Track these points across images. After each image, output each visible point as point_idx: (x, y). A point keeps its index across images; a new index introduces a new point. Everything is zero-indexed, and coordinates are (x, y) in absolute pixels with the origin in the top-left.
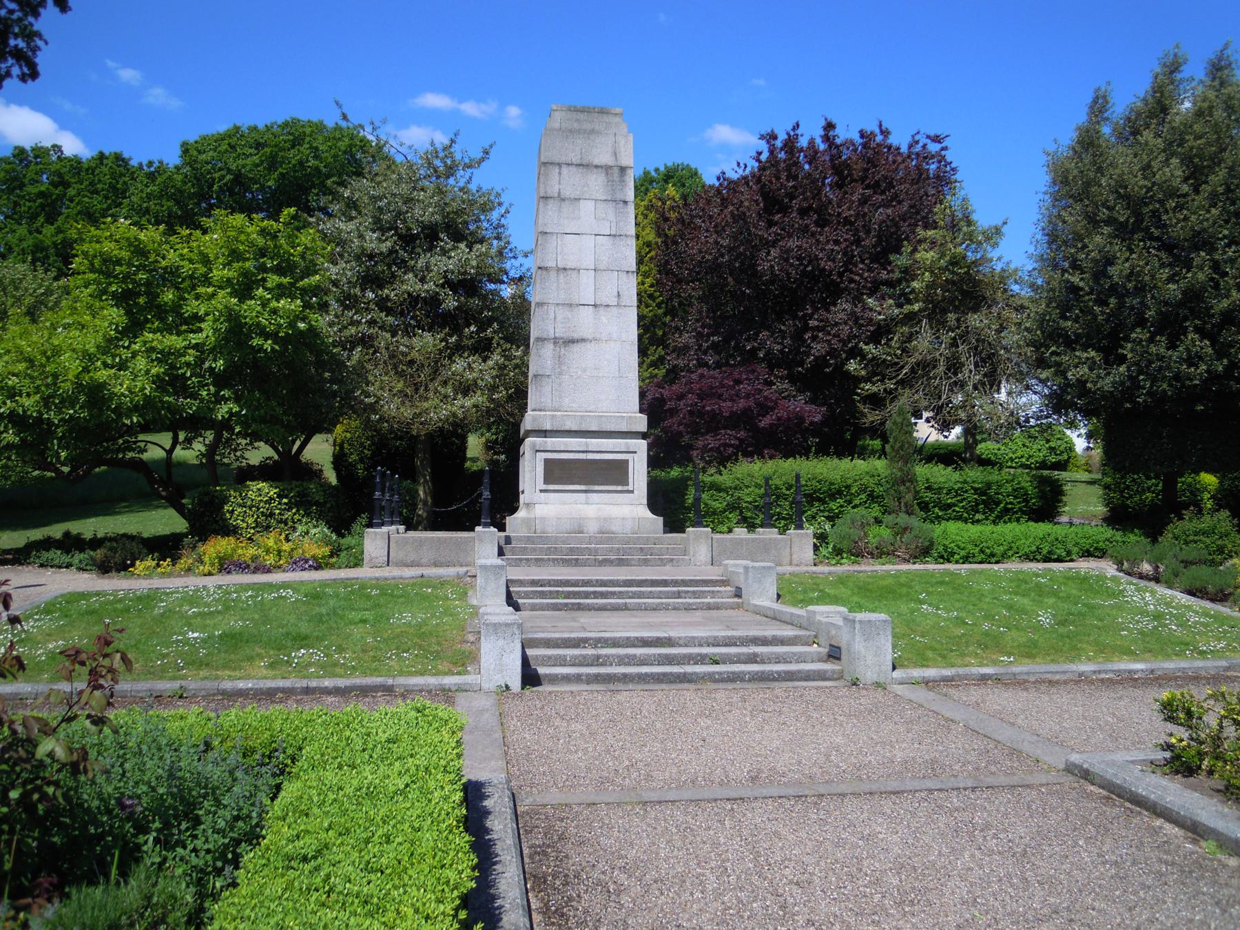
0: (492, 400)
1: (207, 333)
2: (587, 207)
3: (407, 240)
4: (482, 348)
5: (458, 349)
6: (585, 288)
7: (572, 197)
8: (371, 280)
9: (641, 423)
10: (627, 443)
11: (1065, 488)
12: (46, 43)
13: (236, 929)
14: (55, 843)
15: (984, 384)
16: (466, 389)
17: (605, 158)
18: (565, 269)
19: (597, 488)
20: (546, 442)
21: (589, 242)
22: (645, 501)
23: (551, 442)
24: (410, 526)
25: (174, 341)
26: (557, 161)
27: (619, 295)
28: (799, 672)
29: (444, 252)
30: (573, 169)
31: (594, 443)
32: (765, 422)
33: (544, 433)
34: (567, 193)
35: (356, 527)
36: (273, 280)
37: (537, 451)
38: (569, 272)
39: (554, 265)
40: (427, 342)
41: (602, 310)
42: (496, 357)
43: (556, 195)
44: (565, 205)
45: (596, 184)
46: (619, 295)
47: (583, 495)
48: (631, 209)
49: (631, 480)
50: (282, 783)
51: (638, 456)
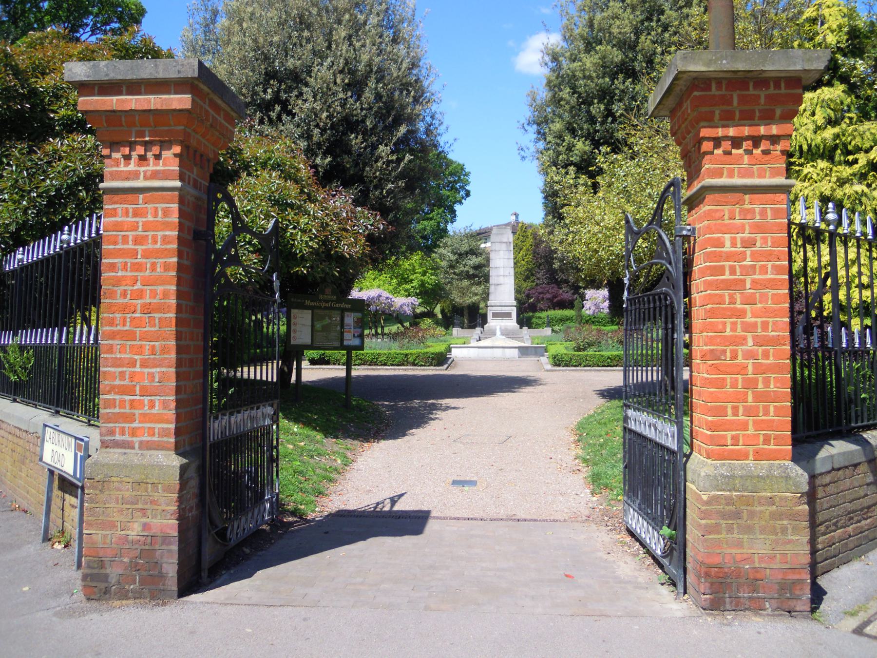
0: (396, 402)
1: (415, 283)
2: (501, 253)
3: (460, 255)
4: (479, 284)
5: (472, 284)
6: (501, 272)
8: (452, 267)
9: (515, 303)
14: (265, 530)
15: (112, 432)
16: (476, 294)
17: (505, 240)
21: (502, 260)
23: (493, 308)
24: (462, 328)
25: (408, 286)
29: (470, 259)
31: (503, 308)
32: (556, 300)
33: (492, 306)
35: (450, 328)
36: (430, 271)
40: (466, 283)
42: (483, 286)
45: (504, 246)
48: (512, 252)
50: (449, 350)
51: (514, 312)
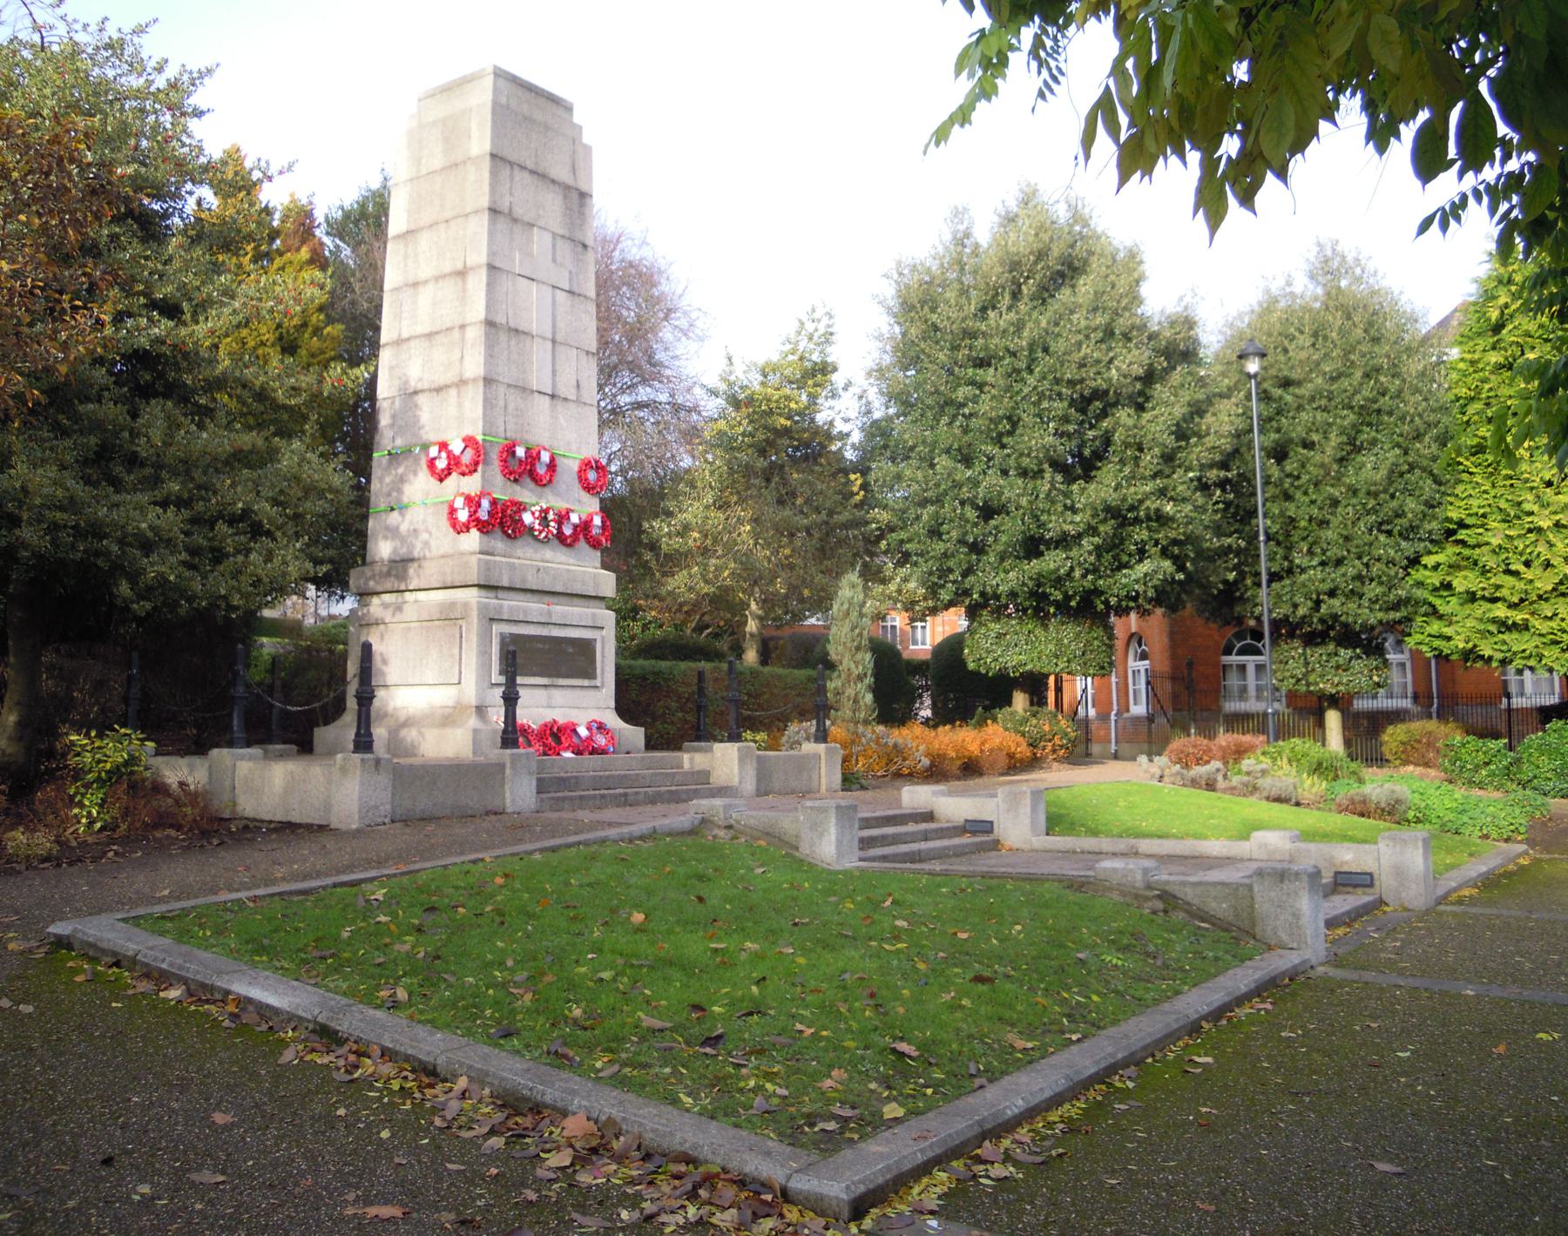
7: (526, 218)
10: (594, 615)
11: (821, 418)
12: (259, 160)
13: (468, 1235)
18: (516, 331)
19: (562, 682)
20: (501, 607)
22: (613, 704)
26: (509, 157)
27: (578, 386)
28: (950, 837)
30: (526, 175)
31: (561, 610)
34: (519, 212)
37: (492, 619)
38: (522, 337)
39: (504, 322)
41: (560, 405)
43: (506, 211)
44: (517, 229)
46: (578, 386)
47: (542, 692)
49: (599, 671)
